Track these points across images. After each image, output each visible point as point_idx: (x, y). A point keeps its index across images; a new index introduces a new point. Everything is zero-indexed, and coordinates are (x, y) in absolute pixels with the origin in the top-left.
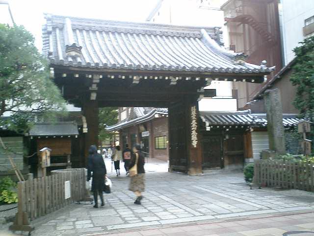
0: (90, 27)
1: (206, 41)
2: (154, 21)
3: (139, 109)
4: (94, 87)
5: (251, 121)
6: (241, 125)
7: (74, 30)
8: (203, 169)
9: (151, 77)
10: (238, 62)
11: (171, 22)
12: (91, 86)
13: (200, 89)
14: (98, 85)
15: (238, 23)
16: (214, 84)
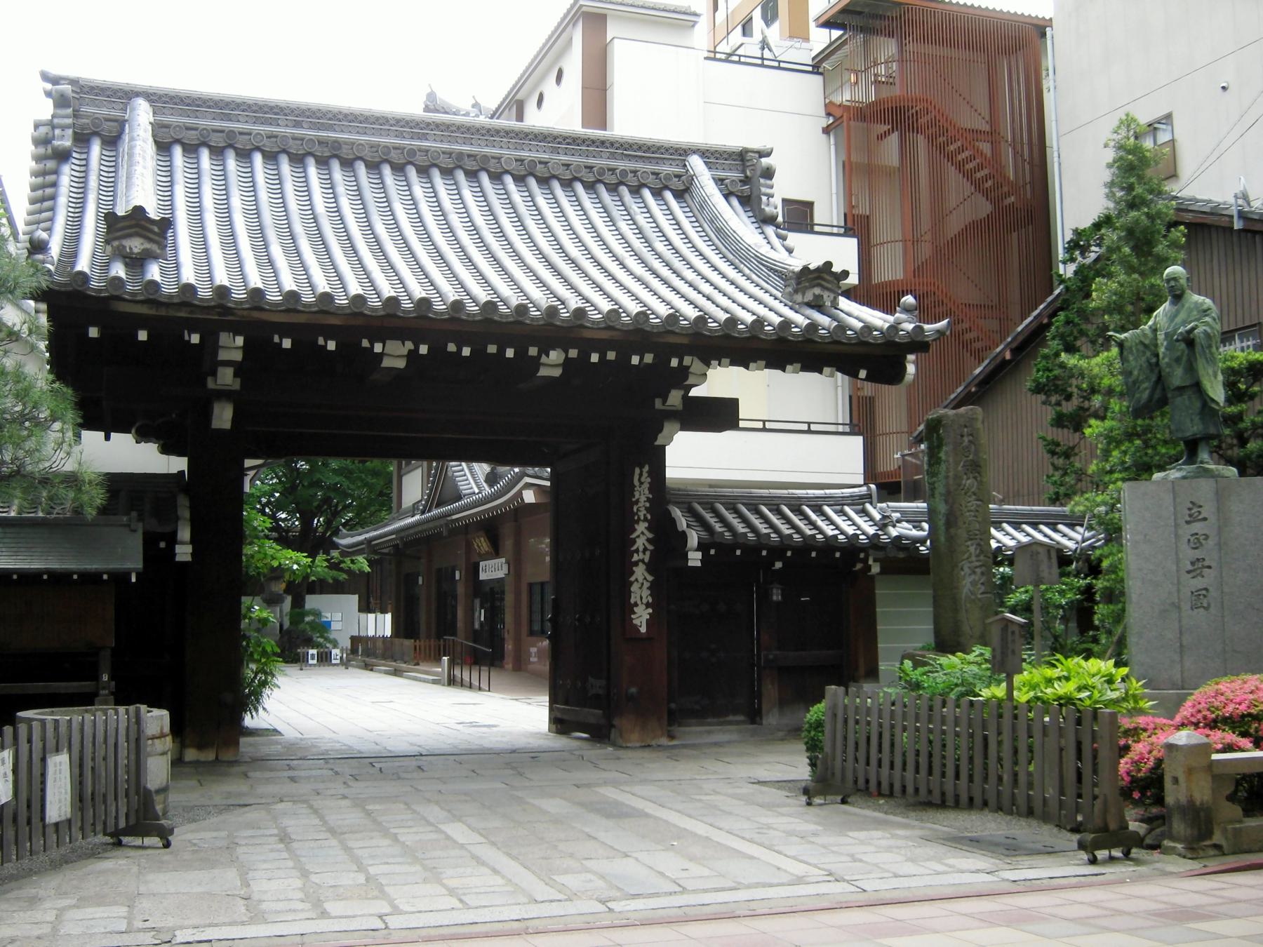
0: (337, 144)
1: (703, 205)
3: (470, 470)
4: (226, 378)
5: (871, 531)
6: (830, 543)
7: (163, 147)
8: (670, 724)
9: (492, 349)
10: (809, 296)
12: (214, 374)
14: (239, 368)
16: (720, 381)
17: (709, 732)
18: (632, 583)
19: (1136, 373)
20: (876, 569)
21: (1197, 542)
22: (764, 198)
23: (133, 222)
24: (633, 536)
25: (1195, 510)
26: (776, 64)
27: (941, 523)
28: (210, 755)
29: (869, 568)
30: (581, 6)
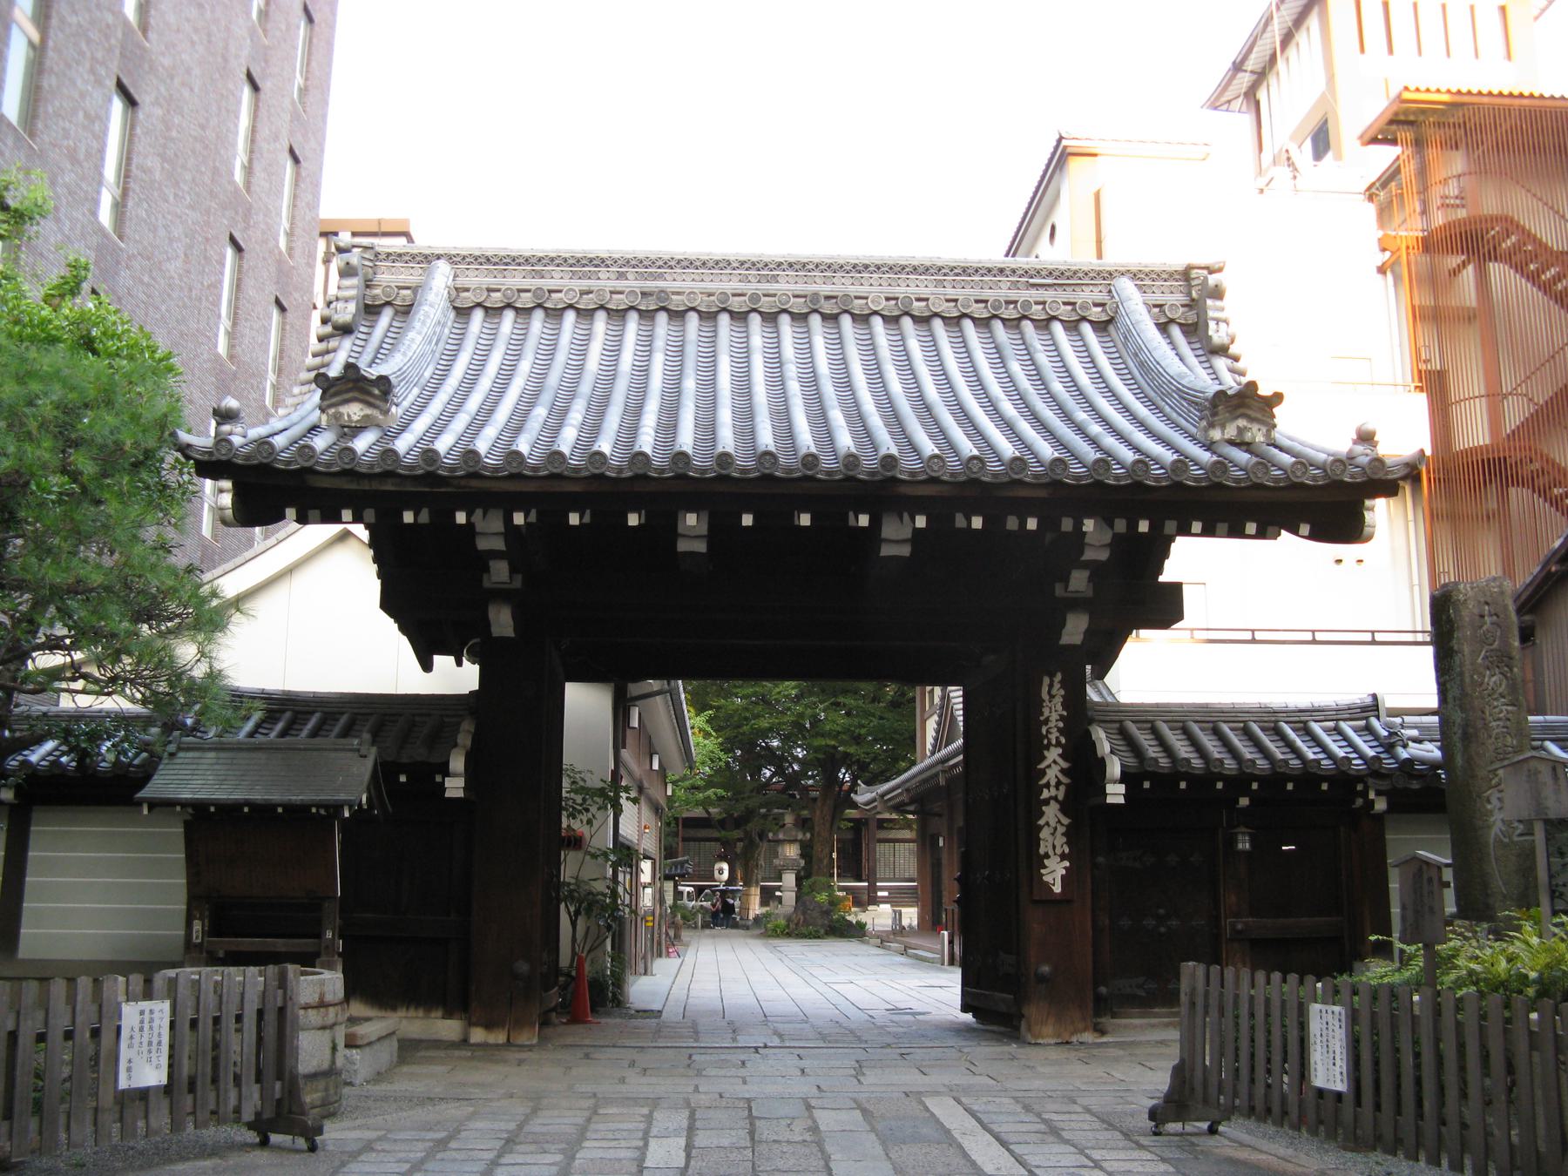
4: (500, 572)
8: (1097, 1014)
10: (1231, 431)
11: (1100, 256)
12: (487, 569)
15: (1454, 261)
18: (1040, 828)
20: (1381, 805)
22: (1212, 325)
24: (1042, 766)
28: (499, 1037)
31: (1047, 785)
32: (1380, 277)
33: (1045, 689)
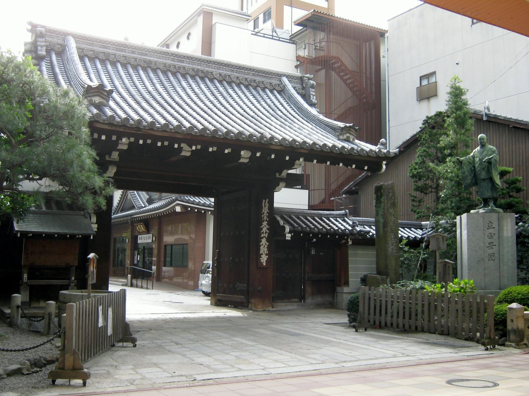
0: (150, 62)
2: (178, 46)
6: (336, 233)
7: (82, 58)
8: (273, 301)
10: (345, 137)
13: (280, 173)
17: (286, 305)
18: (261, 246)
19: (466, 173)
20: (350, 243)
21: (491, 236)
23: (97, 90)
25: (490, 224)
26: (278, 39)
27: (381, 225)
29: (348, 242)
30: (203, 8)
31: (263, 233)
32: (295, 69)
33: (263, 203)
